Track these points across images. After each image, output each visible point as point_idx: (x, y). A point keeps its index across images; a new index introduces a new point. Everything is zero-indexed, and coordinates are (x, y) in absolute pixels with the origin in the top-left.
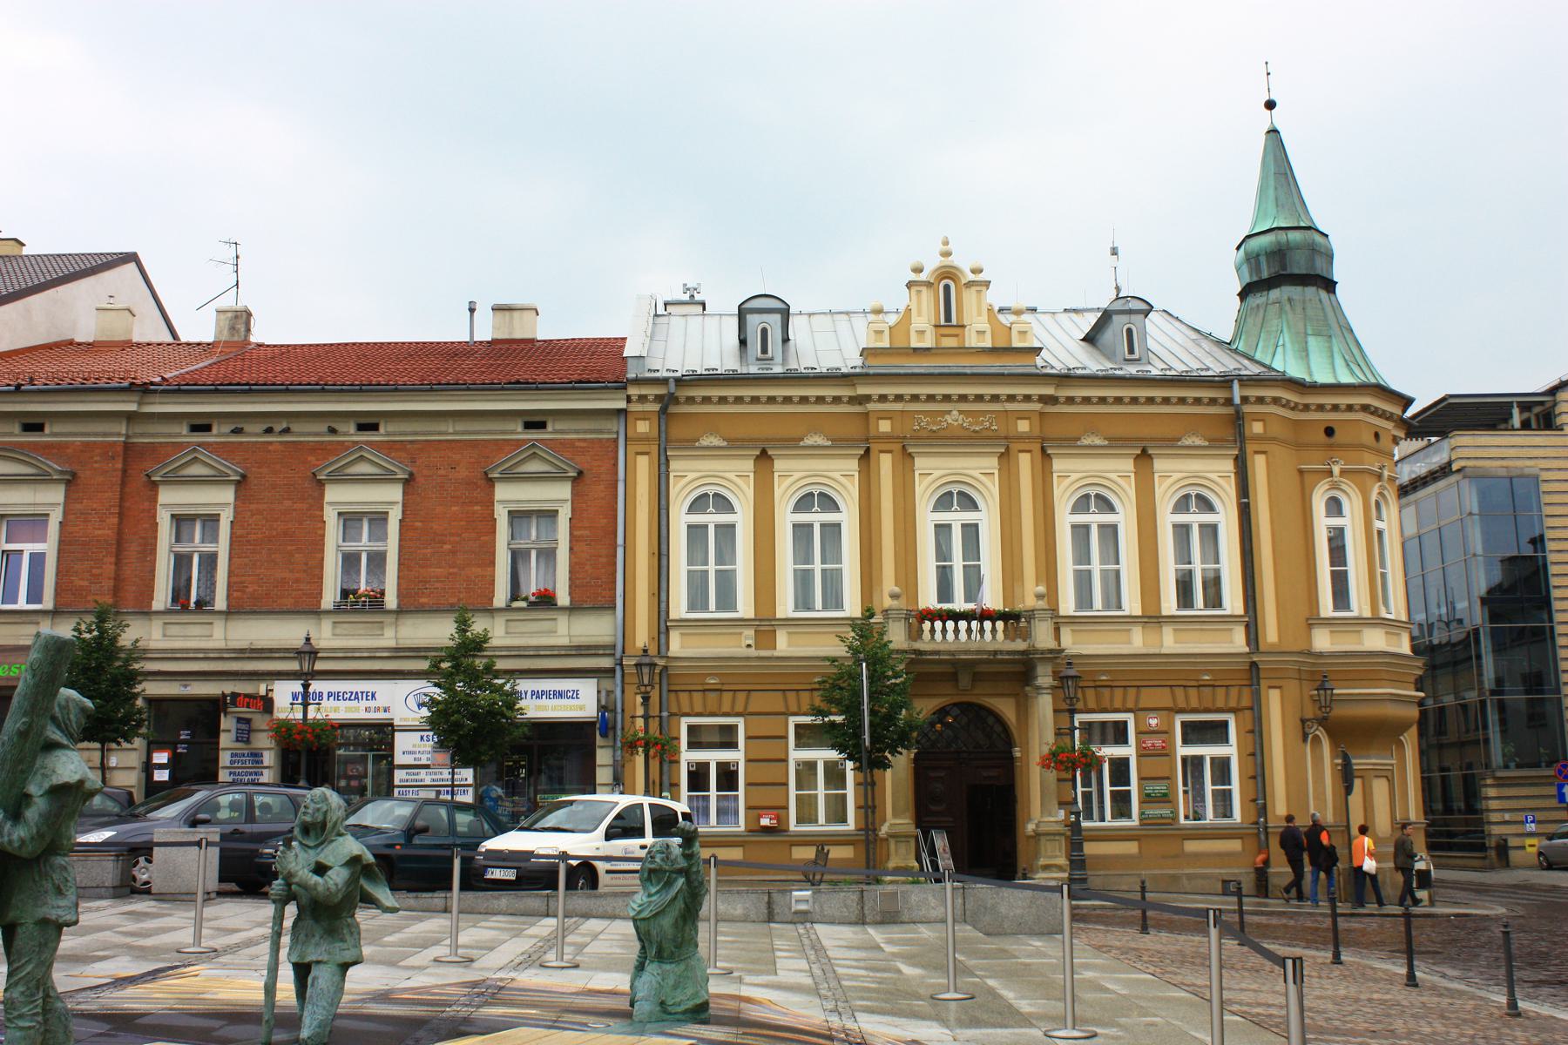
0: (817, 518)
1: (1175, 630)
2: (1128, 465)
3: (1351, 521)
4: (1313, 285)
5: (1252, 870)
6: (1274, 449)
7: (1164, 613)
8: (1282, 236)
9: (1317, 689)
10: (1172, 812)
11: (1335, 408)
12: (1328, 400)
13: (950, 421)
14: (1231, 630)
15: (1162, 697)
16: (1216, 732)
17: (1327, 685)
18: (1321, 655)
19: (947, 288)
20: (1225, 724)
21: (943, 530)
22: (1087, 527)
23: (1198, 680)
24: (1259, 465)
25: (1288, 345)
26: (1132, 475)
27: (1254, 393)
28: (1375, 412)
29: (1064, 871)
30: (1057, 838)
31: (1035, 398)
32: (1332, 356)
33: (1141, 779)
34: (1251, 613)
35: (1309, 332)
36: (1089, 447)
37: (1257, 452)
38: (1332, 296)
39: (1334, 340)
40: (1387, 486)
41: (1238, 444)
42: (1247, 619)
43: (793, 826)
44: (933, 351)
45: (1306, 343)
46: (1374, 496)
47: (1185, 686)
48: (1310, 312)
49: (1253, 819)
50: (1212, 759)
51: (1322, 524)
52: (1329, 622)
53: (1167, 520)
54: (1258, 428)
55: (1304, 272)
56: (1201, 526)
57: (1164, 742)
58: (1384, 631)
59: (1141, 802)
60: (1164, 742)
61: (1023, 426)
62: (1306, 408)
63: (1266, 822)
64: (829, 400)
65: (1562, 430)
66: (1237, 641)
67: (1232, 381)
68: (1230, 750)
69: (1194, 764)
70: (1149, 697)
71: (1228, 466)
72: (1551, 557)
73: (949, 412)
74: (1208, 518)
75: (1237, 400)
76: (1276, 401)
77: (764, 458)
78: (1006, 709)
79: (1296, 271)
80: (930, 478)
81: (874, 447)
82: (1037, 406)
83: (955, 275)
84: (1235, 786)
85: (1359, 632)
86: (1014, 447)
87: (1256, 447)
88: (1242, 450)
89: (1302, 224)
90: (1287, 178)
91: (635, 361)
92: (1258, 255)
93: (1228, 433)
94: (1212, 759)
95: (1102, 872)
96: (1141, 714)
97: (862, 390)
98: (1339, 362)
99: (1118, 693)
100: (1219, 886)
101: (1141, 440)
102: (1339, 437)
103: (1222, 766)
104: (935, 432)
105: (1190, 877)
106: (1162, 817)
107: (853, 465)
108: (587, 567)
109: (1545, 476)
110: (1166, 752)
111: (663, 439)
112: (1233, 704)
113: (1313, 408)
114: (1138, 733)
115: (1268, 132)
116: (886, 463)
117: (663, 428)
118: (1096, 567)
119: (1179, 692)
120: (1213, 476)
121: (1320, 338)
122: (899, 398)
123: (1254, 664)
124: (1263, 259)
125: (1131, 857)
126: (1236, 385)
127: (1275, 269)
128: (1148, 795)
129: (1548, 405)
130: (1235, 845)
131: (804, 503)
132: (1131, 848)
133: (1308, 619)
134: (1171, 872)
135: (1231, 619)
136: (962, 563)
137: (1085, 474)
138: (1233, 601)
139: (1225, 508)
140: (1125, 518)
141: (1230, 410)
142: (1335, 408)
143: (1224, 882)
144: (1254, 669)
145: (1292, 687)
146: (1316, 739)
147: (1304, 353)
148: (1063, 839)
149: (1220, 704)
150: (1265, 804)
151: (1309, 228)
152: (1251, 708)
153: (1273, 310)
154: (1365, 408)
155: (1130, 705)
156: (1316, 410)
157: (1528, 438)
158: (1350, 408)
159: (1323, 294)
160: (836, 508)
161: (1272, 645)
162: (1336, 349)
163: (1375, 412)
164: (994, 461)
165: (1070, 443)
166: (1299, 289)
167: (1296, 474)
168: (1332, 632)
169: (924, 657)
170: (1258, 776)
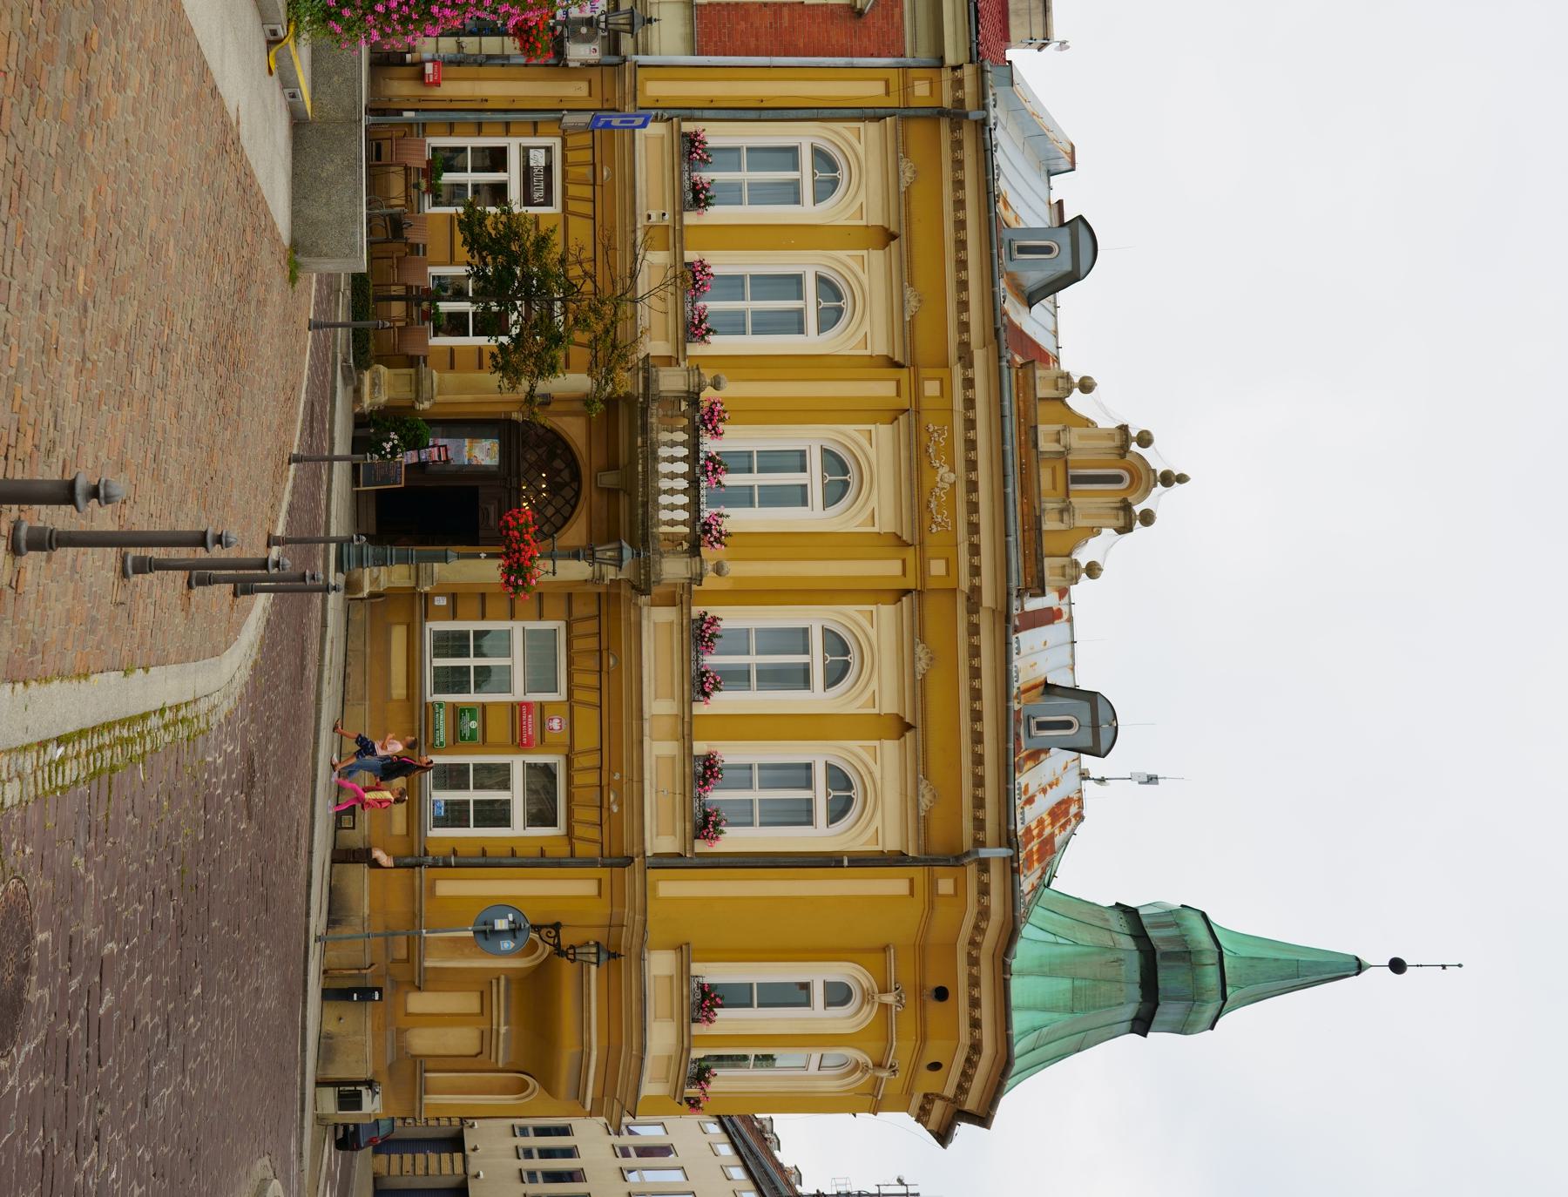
0: (820, 794)
2: (889, 705)
8: (1209, 959)
10: (441, 744)
11: (975, 1003)
13: (941, 471)
14: (674, 834)
15: (587, 738)
16: (541, 815)
18: (641, 959)
19: (1119, 480)
20: (553, 823)
21: (798, 461)
22: (808, 784)
24: (892, 885)
25: (1057, 950)
26: (876, 711)
27: (995, 878)
28: (970, 1063)
29: (377, 371)
31: (976, 581)
32: (1045, 1009)
33: (484, 706)
34: (697, 861)
35: (1076, 982)
37: (912, 881)
38: (1127, 1025)
39: (1067, 1017)
40: (868, 1076)
41: (923, 857)
43: (435, 626)
47: (601, 768)
50: (507, 802)
51: (818, 974)
53: (817, 754)
54: (946, 886)
55: (1161, 985)
56: (809, 801)
59: (454, 705)
61: (937, 568)
62: (974, 961)
64: (975, 561)
66: (662, 839)
67: (1010, 845)
68: (519, 828)
71: (892, 843)
73: (952, 470)
75: (984, 853)
76: (984, 913)
77: (903, 727)
78: (575, 533)
79: (1161, 975)
80: (865, 443)
81: (903, 374)
82: (964, 585)
84: (472, 832)
86: (910, 554)
88: (915, 862)
89: (1229, 990)
90: (1291, 977)
91: (1008, 74)
92: (1178, 925)
95: (368, 650)
96: (566, 708)
97: (979, 356)
98: (1039, 1018)
101: (924, 719)
102: (934, 1007)
104: (928, 507)
106: (436, 730)
107: (880, 347)
108: (743, 23)
110: (520, 744)
111: (906, 112)
112: (579, 831)
113: (974, 971)
115: (1357, 959)
116: (888, 569)
117: (921, 112)
118: (749, 305)
119: (594, 760)
120: (877, 822)
121: (1069, 995)
122: (970, 404)
126: (1005, 852)
127: (1162, 947)
131: (838, 778)
132: (399, 690)
133: (687, 944)
136: (756, 483)
137: (879, 782)
140: (816, 699)
142: (975, 1003)
145: (600, 912)
147: (1048, 970)
148: (412, 584)
150: (451, 867)
151: (1224, 997)
152: (572, 855)
154: (976, 1048)
155: (578, 695)
156: (970, 975)
158: (975, 1024)
159: (1130, 1011)
160: (821, 329)
161: (655, 889)
162: (1056, 1016)
163: (970, 1063)
165: (918, 631)
166: (1137, 978)
170: (484, 861)
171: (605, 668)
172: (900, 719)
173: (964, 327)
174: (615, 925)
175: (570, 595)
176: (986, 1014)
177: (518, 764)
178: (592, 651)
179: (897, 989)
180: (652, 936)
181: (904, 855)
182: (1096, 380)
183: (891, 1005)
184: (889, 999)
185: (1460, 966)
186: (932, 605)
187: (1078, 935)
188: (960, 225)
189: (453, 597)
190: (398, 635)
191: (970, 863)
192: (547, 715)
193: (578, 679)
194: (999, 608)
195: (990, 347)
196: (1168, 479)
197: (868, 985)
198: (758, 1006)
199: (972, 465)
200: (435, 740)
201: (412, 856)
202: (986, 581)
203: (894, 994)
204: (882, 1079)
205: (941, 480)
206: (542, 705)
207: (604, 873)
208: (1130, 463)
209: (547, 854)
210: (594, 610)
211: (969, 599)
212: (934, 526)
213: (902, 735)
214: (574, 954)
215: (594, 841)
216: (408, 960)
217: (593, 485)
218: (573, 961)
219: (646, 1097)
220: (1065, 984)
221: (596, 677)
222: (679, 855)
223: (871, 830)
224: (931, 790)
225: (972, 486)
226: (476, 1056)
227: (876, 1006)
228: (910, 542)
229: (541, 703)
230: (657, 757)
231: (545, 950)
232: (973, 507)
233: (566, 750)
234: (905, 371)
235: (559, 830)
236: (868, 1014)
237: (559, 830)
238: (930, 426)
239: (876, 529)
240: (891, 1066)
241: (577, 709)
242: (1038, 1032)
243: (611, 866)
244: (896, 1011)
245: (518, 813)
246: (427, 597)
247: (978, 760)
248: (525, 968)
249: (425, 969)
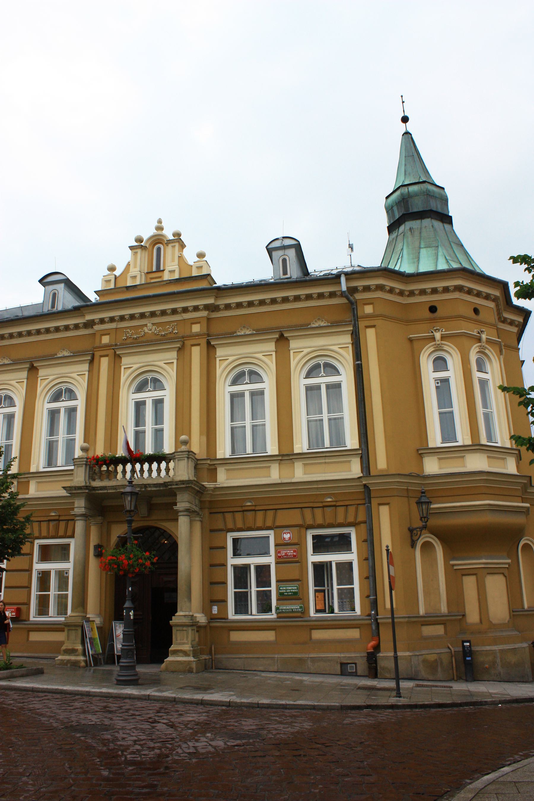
1: (305, 465)
2: (271, 346)
4: (428, 218)
5: (366, 655)
6: (378, 322)
8: (405, 190)
10: (301, 607)
11: (434, 291)
13: (146, 331)
15: (295, 517)
21: (140, 406)
23: (322, 502)
26: (274, 354)
27: (360, 283)
30: (185, 628)
35: (422, 246)
36: (245, 336)
37: (367, 327)
39: (440, 248)
43: (231, 615)
44: (138, 287)
45: (419, 253)
46: (473, 357)
47: (313, 508)
48: (424, 234)
49: (367, 613)
50: (337, 564)
52: (436, 451)
54: (369, 309)
55: (421, 209)
57: (294, 551)
58: (486, 456)
59: (278, 600)
60: (294, 551)
61: (196, 328)
62: (412, 293)
63: (377, 614)
68: (69, 566)
70: (283, 518)
71: (347, 339)
73: (146, 325)
78: (167, 526)
79: (415, 210)
82: (205, 313)
83: (159, 239)
84: (356, 586)
87: (368, 323)
89: (421, 181)
92: (392, 207)
93: (348, 317)
94: (337, 564)
95: (244, 656)
99: (260, 514)
100: (338, 667)
102: (440, 312)
103: (62, 576)
105: (313, 660)
106: (292, 611)
112: (351, 519)
115: (403, 135)
119: (308, 513)
120: (335, 348)
121: (429, 249)
122: (112, 320)
124: (395, 208)
125: (438, 637)
126: (343, 279)
128: (282, 594)
130: (354, 634)
132: (270, 636)
133: (418, 450)
134: (299, 656)
135: (351, 452)
142: (434, 291)
143: (342, 664)
149: (340, 519)
150: (376, 599)
151: (424, 182)
152: (365, 522)
153: (400, 238)
158: (446, 290)
159: (438, 224)
161: (382, 470)
162: (440, 254)
164: (174, 354)
166: (418, 222)
168: (440, 459)
169: (97, 492)
171: (253, 508)
173: (77, 327)
174: (407, 494)
175: (212, 531)
176: (440, 285)
177: (313, 558)
178: (276, 513)
179: (432, 332)
180: (414, 470)
181: (353, 332)
183: (441, 334)
184: (438, 335)
185: (402, 96)
186: (216, 329)
187: (399, 249)
188: (29, 333)
189: (213, 602)
190: (236, 636)
191: (355, 298)
192: (281, 542)
193: (259, 524)
194: (214, 294)
195: (84, 312)
196: (160, 228)
197: (432, 348)
198: (452, 408)
199: (142, 316)
200: (298, 612)
201: (371, 624)
202: (200, 302)
203: (435, 333)
204: (487, 338)
205: (151, 330)
206: (276, 545)
207: (374, 502)
208: (150, 245)
209: (366, 538)
210: (220, 516)
211: (213, 311)
212: (174, 332)
215: (357, 509)
217: (147, 519)
219: (518, 471)
220: (423, 252)
221: (258, 512)
222: (361, 458)
224: (316, 321)
225: (153, 314)
226: (505, 576)
227: (443, 342)
228: (181, 343)
229: (275, 546)
230: (305, 474)
231: (426, 537)
232: (164, 313)
233: (303, 530)
234: (95, 353)
235: (353, 533)
236: (449, 346)
237: (353, 533)
238: (123, 338)
239: (175, 361)
240: (479, 333)
241: (278, 523)
242: (449, 261)
243: (370, 498)
244: (445, 332)
246: (212, 618)
247: (297, 298)
248: (443, 547)
249: (449, 612)
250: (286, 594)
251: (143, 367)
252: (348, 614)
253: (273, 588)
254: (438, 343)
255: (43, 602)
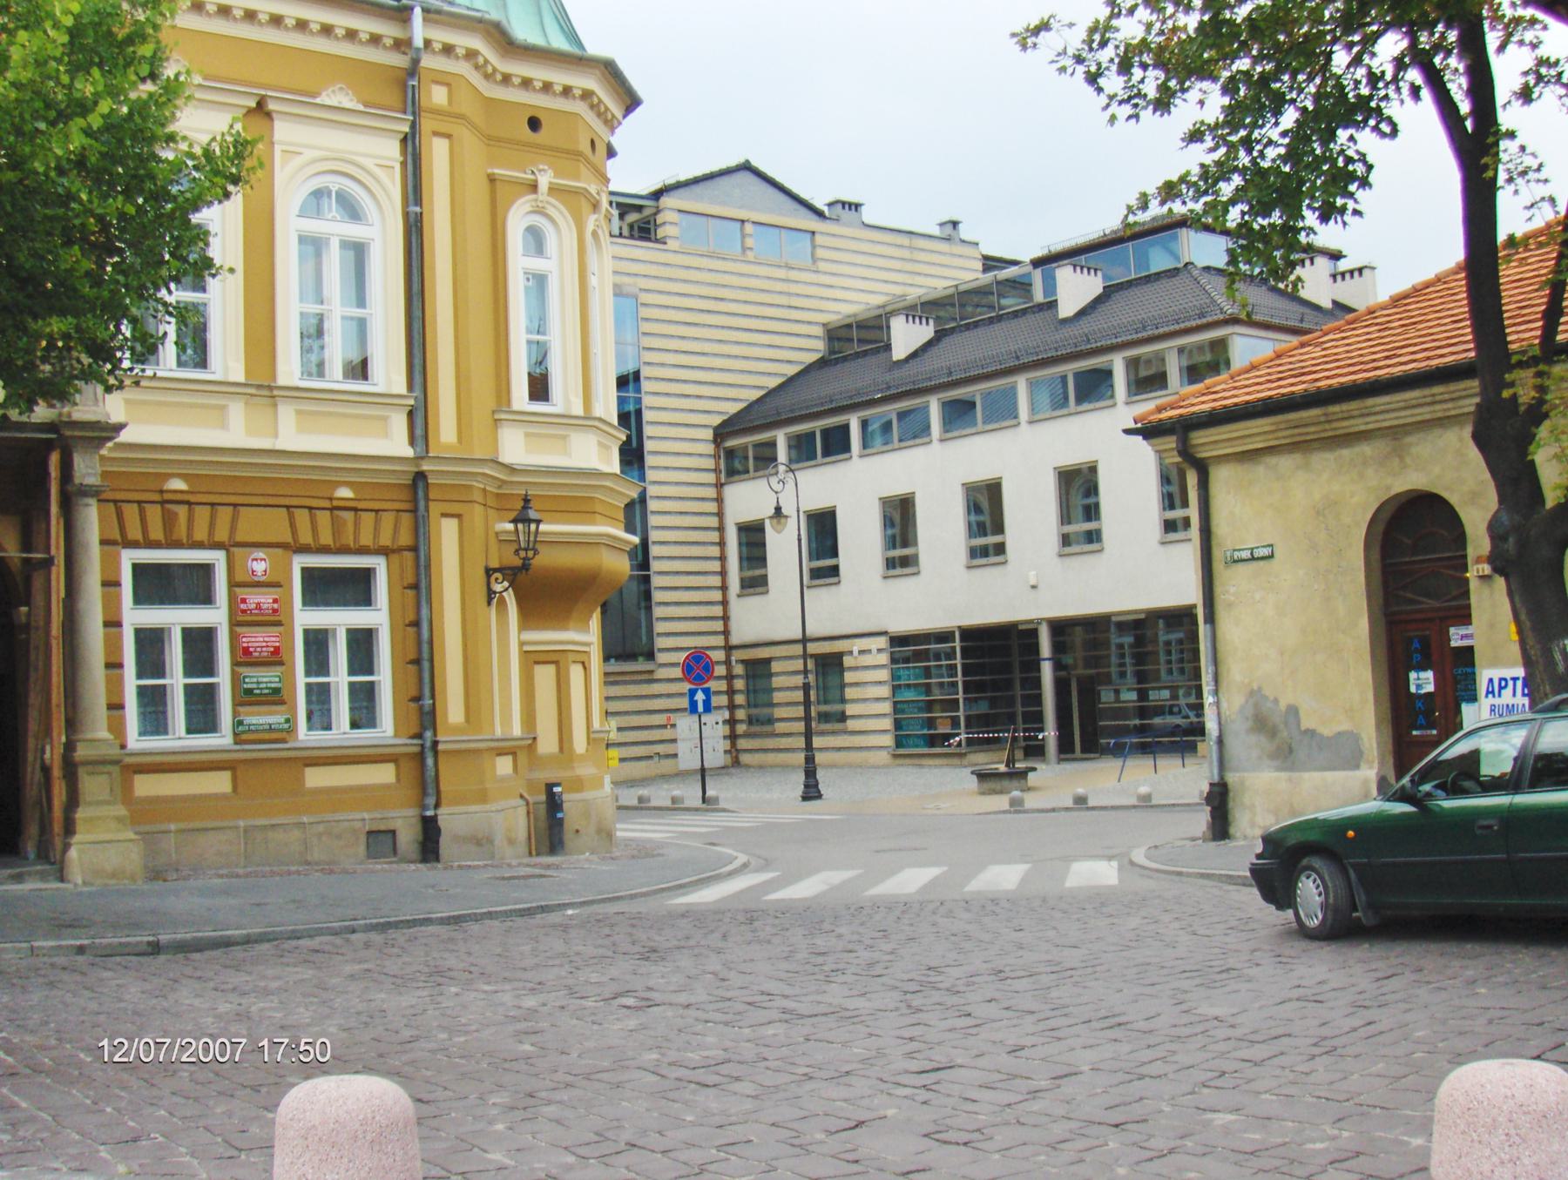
3: (557, 262)
7: (281, 381)
9: (515, 521)
10: (288, 721)
12: (539, 73)
14: (564, 437)
15: (274, 525)
16: (354, 588)
17: (532, 514)
18: (511, 469)
20: (366, 575)
24: (438, 154)
27: (441, 36)
37: (436, 134)
42: (412, 402)
51: (519, 262)
52: (523, 418)
59: (237, 703)
65: (665, 243)
66: (394, 442)
68: (377, 617)
69: (317, 642)
70: (253, 524)
71: (391, 150)
72: (647, 401)
74: (355, 231)
85: (564, 437)
93: (393, 98)
103: (199, 644)
106: (271, 729)
109: (645, 298)
110: (276, 619)
112: (385, 540)
114: (233, 584)
123: (420, 476)
128: (249, 692)
129: (647, 212)
130: (384, 774)
132: (219, 783)
135: (384, 400)
138: (389, 374)
139: (383, 219)
141: (400, 61)
144: (421, 485)
146: (502, 602)
149: (366, 540)
152: (409, 549)
157: (629, 250)
167: (485, 181)
172: (250, 112)
177: (306, 618)
182: (1086, 85)
192: (248, 579)
200: (282, 730)
213: (269, 115)
214: (526, 550)
216: (514, 754)
218: (536, 552)
222: (411, 414)
223: (378, 171)
224: (334, 92)
235: (379, 564)
245: (196, 616)
250: (258, 692)
251: (327, 159)
252: (364, 736)
253: (301, 680)
254: (541, 198)
255: (153, 701)
